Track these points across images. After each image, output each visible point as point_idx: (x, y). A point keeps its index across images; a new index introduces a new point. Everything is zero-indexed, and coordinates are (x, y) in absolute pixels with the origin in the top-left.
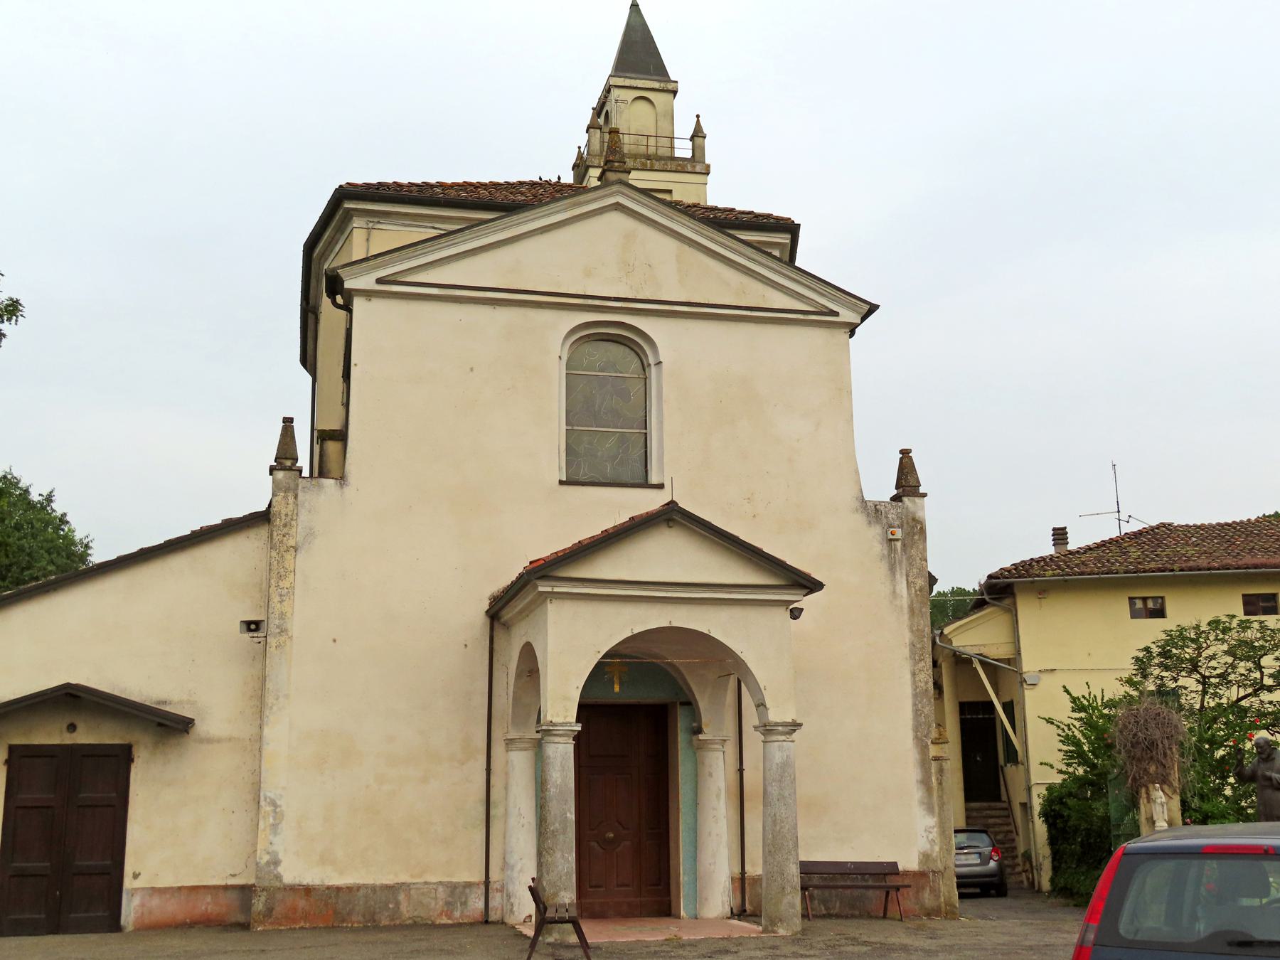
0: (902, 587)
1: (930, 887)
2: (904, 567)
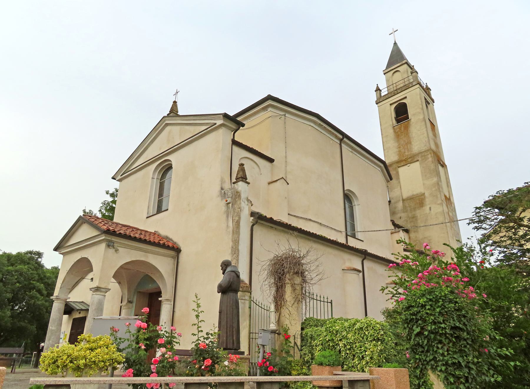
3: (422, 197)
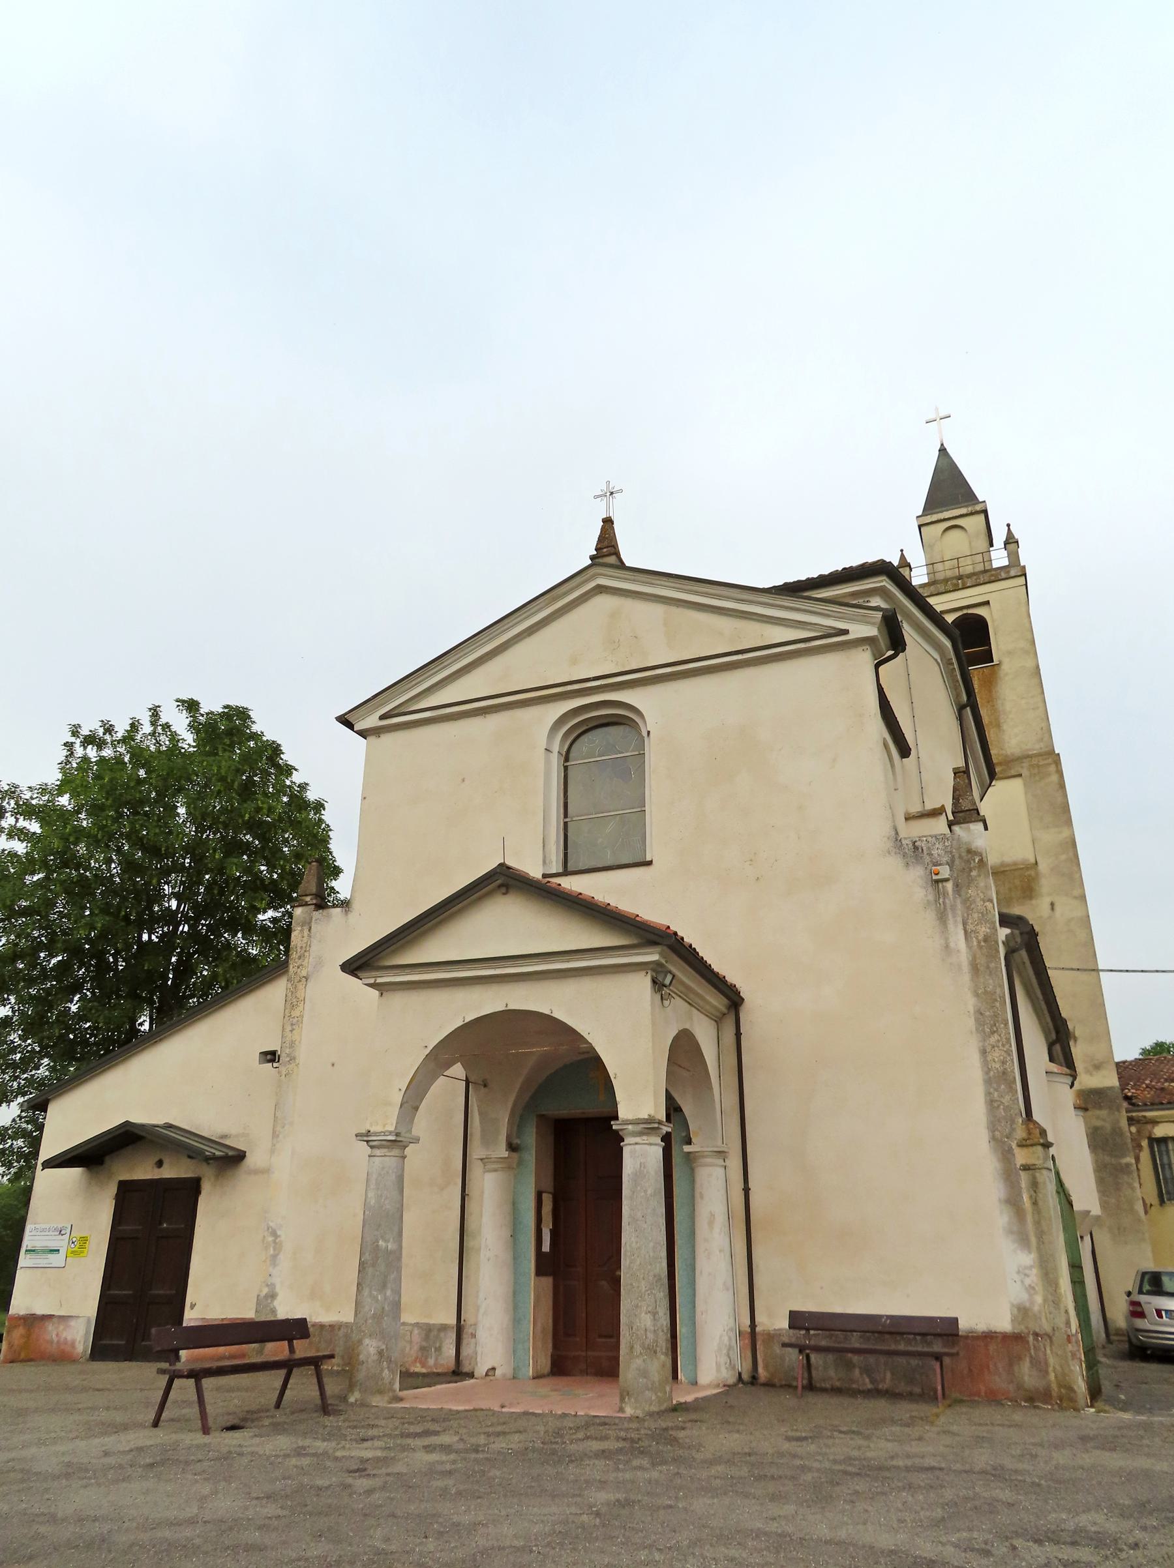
0: (958, 939)
1: (1031, 1357)
2: (959, 912)
3: (1029, 873)
